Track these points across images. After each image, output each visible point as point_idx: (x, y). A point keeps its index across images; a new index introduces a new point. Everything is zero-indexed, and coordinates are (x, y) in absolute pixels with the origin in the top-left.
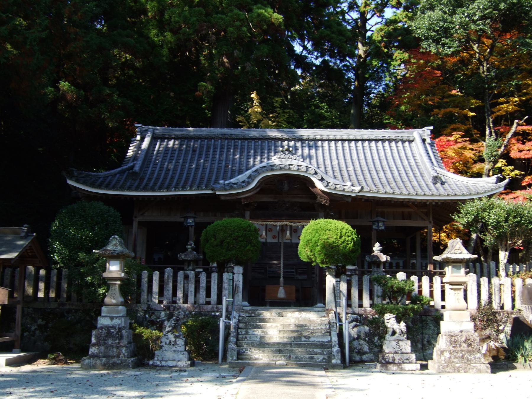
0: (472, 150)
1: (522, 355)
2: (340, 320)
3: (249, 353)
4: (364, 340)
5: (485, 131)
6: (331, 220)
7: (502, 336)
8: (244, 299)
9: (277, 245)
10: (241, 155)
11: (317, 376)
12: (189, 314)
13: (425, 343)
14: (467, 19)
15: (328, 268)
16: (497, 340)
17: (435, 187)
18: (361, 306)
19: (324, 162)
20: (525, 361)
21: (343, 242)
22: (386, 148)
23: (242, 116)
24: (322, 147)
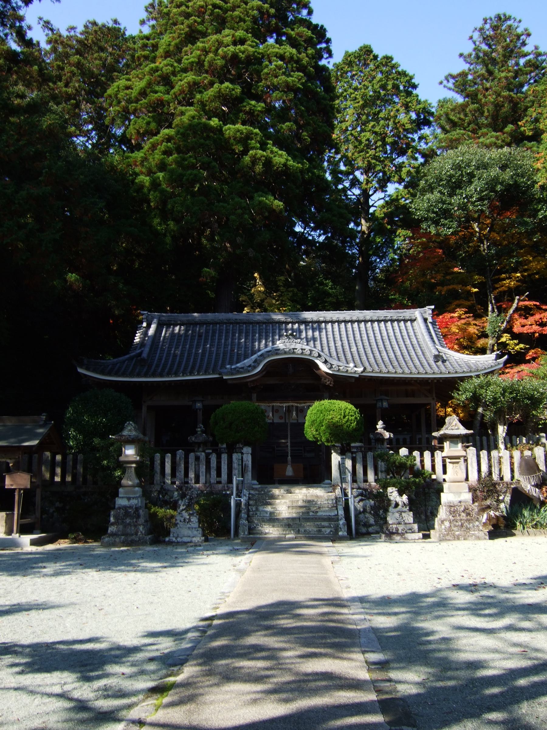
0: (476, 325)
1: (521, 523)
2: (346, 495)
3: (260, 528)
4: (370, 513)
5: (488, 307)
6: (335, 401)
7: (502, 506)
8: (253, 478)
9: (285, 425)
10: (246, 339)
11: (325, 546)
12: (201, 493)
13: (429, 514)
14: (466, 200)
15: (334, 446)
16: (497, 509)
17: (437, 365)
18: (366, 481)
19: (328, 344)
20: (524, 528)
21: (347, 422)
22: (388, 328)
23: (245, 295)
24: (326, 329)
